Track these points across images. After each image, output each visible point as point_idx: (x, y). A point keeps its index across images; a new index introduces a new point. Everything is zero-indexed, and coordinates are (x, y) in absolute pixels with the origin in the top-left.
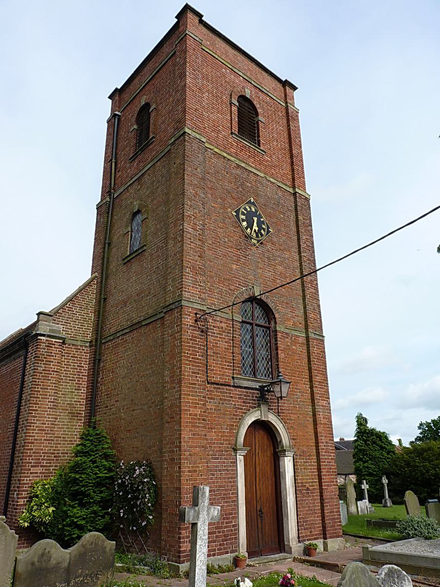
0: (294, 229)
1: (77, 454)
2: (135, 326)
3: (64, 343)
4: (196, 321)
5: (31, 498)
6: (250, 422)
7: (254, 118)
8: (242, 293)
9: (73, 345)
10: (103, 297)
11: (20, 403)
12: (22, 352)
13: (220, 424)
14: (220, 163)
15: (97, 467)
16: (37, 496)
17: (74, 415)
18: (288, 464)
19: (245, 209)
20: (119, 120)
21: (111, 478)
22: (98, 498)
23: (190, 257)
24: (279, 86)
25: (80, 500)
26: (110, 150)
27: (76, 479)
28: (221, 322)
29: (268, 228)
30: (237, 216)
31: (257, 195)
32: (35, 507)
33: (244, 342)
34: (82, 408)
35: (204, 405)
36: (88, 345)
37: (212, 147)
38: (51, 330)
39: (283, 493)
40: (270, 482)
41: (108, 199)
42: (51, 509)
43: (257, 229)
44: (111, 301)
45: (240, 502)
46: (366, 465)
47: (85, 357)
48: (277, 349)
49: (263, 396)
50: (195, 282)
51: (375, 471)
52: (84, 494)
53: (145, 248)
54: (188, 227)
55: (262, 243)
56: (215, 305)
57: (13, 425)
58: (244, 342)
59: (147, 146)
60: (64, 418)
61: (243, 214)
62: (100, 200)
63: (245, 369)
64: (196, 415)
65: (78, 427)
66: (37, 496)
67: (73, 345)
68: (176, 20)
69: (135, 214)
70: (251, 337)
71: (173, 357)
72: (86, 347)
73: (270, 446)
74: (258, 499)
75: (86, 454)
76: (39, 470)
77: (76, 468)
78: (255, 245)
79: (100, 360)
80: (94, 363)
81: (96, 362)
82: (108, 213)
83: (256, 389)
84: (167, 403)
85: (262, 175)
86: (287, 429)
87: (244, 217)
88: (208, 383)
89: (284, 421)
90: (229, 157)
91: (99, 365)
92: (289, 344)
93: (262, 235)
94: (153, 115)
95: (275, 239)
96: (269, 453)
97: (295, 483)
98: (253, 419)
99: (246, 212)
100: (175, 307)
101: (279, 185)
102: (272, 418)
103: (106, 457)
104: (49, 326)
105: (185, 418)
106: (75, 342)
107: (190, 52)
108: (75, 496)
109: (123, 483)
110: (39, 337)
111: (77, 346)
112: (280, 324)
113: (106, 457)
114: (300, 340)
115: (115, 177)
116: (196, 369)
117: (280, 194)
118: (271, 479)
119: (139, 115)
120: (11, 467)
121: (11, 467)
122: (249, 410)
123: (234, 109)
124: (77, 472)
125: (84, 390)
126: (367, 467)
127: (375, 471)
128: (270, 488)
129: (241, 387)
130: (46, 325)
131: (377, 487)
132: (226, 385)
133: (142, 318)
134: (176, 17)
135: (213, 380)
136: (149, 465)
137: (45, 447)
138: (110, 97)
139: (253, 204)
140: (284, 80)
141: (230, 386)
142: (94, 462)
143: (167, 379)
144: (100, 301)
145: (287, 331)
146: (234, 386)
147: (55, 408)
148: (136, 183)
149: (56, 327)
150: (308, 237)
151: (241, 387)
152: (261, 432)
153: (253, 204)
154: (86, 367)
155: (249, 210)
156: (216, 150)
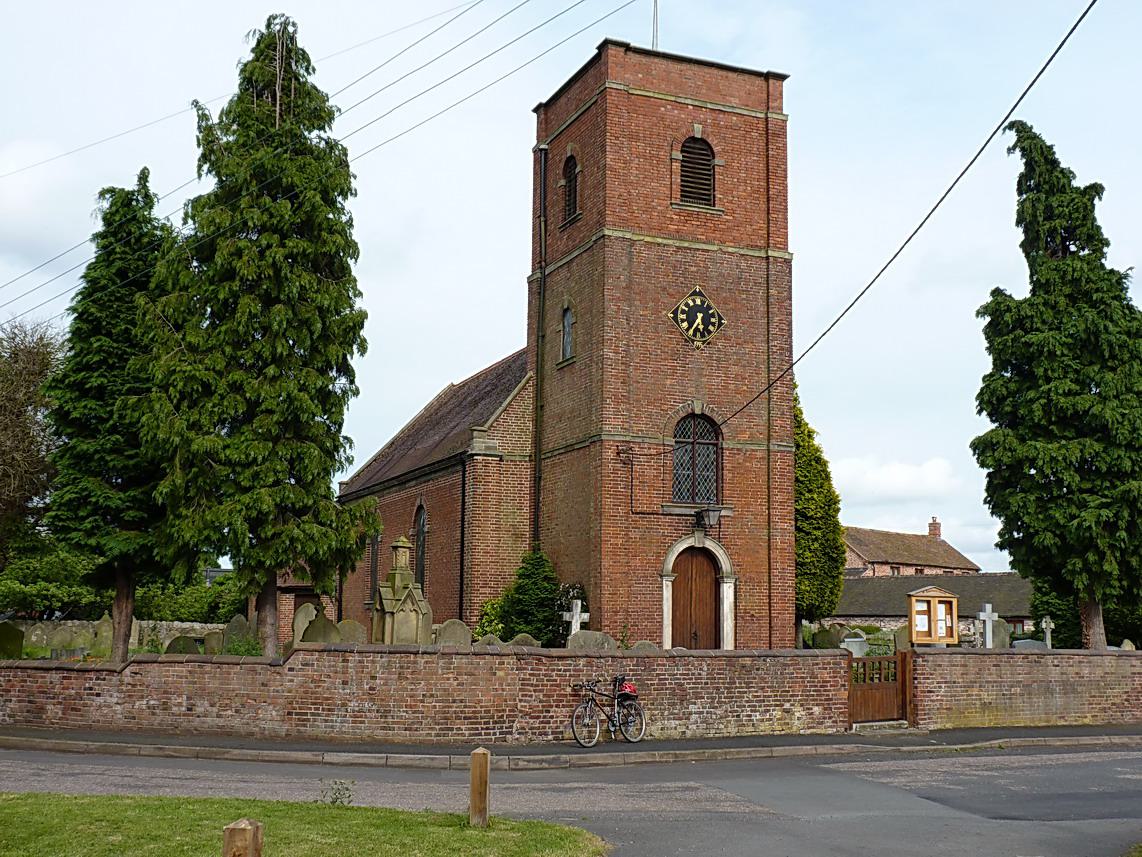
0: (763, 309)
1: (520, 576)
2: (569, 449)
3: (501, 460)
4: (618, 454)
5: (482, 616)
6: (681, 549)
7: (709, 160)
8: (677, 412)
9: (512, 461)
10: (539, 404)
11: (463, 525)
12: (459, 468)
13: (645, 552)
14: (654, 253)
15: (538, 589)
16: (487, 614)
17: (518, 536)
18: (728, 591)
19: (687, 305)
20: (546, 154)
21: (552, 599)
22: (540, 617)
23: (613, 386)
24: (760, 82)
25: (526, 619)
26: (538, 201)
27: (519, 599)
28: (650, 448)
29: (720, 318)
30: (675, 318)
31: (705, 278)
32: (486, 624)
33: (682, 465)
34: (526, 529)
35: (626, 535)
36: (527, 459)
37: (642, 238)
38: (488, 448)
39: (721, 618)
40: (709, 607)
41: (539, 275)
42: (500, 626)
43: (701, 327)
44: (547, 411)
45: (665, 615)
46: (1045, 599)
47: (526, 472)
48: (723, 469)
49: (699, 522)
50: (617, 412)
51: (1060, 610)
52: (527, 612)
53: (575, 359)
54: (608, 353)
55: (709, 344)
56: (642, 431)
57: (459, 546)
58: (682, 465)
59: (574, 221)
60: (507, 538)
61: (683, 312)
62: (530, 273)
63: (681, 494)
64: (617, 544)
65: (524, 547)
66: (487, 614)
67: (512, 461)
68: (597, 51)
69: (566, 311)
70: (691, 458)
71: (596, 489)
72: (526, 462)
73: (711, 572)
74: (693, 621)
75: (528, 576)
76: (488, 590)
77: (519, 589)
78: (698, 348)
79: (540, 478)
80: (535, 480)
81: (537, 479)
82: (540, 293)
83: (691, 515)
84: (592, 533)
85: (715, 248)
86: (730, 556)
87: (684, 316)
88: (633, 513)
89: (726, 548)
90: (665, 242)
91: (539, 483)
92: (741, 461)
93: (710, 332)
94: (579, 179)
95: (730, 333)
96: (709, 579)
97: (736, 609)
98: (685, 546)
99: (687, 309)
100: (594, 440)
101: (742, 252)
102: (710, 545)
103: (546, 578)
104: (483, 442)
105: (606, 548)
106: (513, 458)
107: (612, 111)
108: (521, 614)
109: (561, 603)
110: (475, 457)
111: (515, 461)
112: (729, 439)
113: (546, 578)
114: (759, 454)
115: (546, 242)
116: (617, 502)
117: (743, 265)
118: (711, 604)
119: (564, 170)
120: (462, 588)
121: (462, 588)
122: (681, 537)
123: (676, 166)
124: (520, 594)
125: (526, 510)
126: (1047, 603)
127: (1060, 610)
128: (709, 614)
129: (671, 515)
130: (479, 442)
131: (1061, 636)
132: (653, 514)
133: (574, 441)
134: (598, 48)
135: (638, 510)
136: (582, 588)
137: (491, 569)
138: (536, 110)
139: (700, 294)
140: (765, 71)
141: (657, 514)
142: (535, 583)
143: (592, 510)
144: (536, 408)
145: (739, 446)
146: (662, 514)
147: (498, 529)
148: (565, 269)
149: (491, 443)
150: (783, 317)
151: (671, 515)
152: (700, 558)
153: (700, 294)
154: (528, 484)
155: (692, 304)
156: (648, 239)
